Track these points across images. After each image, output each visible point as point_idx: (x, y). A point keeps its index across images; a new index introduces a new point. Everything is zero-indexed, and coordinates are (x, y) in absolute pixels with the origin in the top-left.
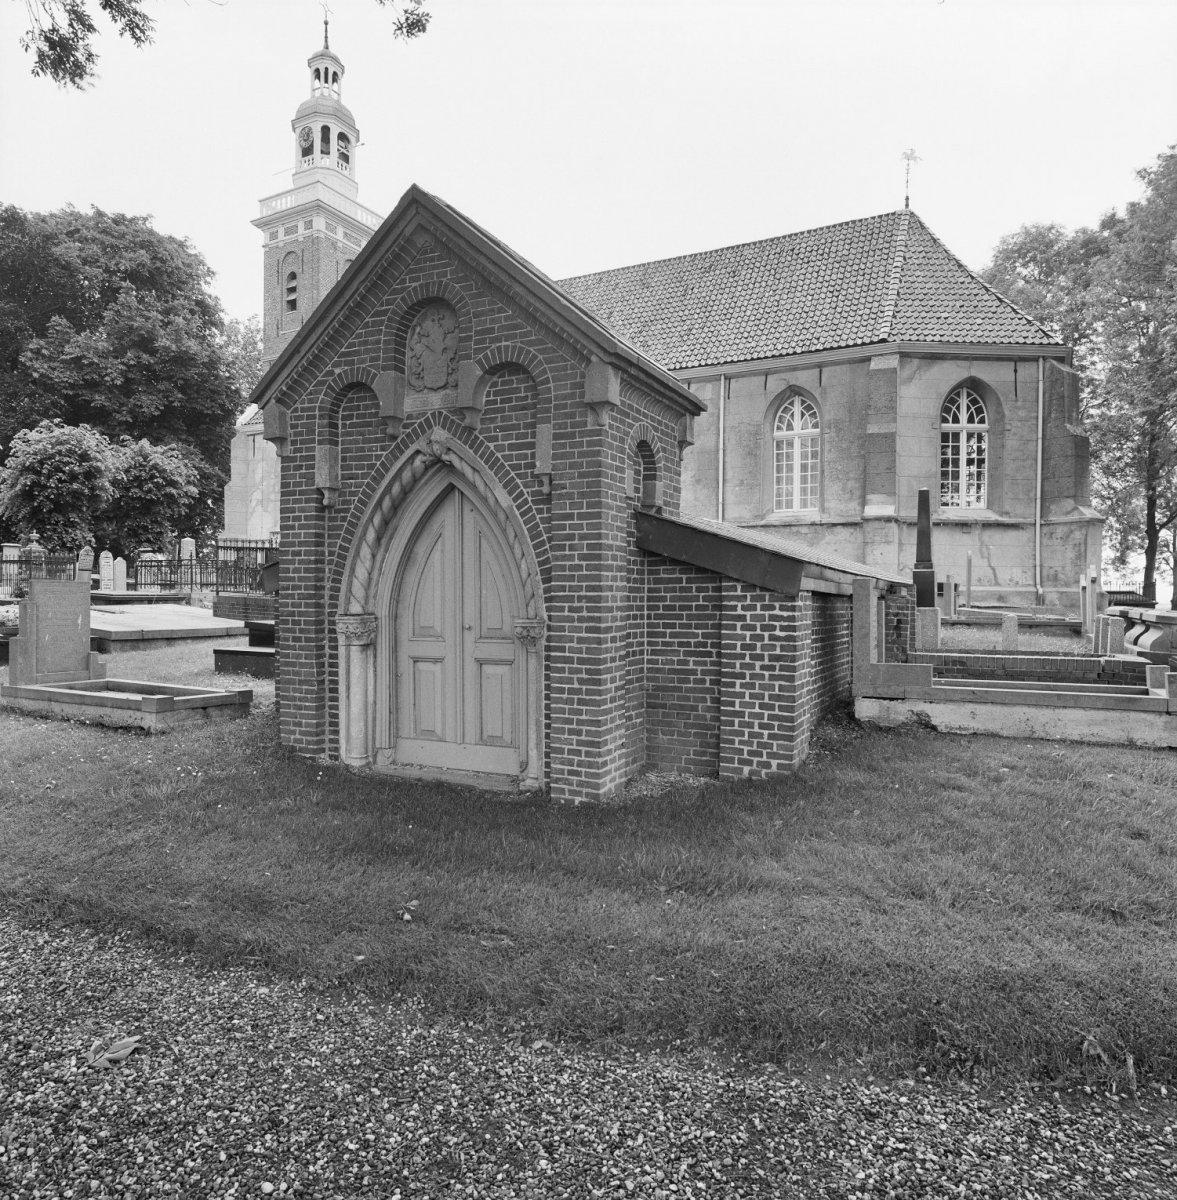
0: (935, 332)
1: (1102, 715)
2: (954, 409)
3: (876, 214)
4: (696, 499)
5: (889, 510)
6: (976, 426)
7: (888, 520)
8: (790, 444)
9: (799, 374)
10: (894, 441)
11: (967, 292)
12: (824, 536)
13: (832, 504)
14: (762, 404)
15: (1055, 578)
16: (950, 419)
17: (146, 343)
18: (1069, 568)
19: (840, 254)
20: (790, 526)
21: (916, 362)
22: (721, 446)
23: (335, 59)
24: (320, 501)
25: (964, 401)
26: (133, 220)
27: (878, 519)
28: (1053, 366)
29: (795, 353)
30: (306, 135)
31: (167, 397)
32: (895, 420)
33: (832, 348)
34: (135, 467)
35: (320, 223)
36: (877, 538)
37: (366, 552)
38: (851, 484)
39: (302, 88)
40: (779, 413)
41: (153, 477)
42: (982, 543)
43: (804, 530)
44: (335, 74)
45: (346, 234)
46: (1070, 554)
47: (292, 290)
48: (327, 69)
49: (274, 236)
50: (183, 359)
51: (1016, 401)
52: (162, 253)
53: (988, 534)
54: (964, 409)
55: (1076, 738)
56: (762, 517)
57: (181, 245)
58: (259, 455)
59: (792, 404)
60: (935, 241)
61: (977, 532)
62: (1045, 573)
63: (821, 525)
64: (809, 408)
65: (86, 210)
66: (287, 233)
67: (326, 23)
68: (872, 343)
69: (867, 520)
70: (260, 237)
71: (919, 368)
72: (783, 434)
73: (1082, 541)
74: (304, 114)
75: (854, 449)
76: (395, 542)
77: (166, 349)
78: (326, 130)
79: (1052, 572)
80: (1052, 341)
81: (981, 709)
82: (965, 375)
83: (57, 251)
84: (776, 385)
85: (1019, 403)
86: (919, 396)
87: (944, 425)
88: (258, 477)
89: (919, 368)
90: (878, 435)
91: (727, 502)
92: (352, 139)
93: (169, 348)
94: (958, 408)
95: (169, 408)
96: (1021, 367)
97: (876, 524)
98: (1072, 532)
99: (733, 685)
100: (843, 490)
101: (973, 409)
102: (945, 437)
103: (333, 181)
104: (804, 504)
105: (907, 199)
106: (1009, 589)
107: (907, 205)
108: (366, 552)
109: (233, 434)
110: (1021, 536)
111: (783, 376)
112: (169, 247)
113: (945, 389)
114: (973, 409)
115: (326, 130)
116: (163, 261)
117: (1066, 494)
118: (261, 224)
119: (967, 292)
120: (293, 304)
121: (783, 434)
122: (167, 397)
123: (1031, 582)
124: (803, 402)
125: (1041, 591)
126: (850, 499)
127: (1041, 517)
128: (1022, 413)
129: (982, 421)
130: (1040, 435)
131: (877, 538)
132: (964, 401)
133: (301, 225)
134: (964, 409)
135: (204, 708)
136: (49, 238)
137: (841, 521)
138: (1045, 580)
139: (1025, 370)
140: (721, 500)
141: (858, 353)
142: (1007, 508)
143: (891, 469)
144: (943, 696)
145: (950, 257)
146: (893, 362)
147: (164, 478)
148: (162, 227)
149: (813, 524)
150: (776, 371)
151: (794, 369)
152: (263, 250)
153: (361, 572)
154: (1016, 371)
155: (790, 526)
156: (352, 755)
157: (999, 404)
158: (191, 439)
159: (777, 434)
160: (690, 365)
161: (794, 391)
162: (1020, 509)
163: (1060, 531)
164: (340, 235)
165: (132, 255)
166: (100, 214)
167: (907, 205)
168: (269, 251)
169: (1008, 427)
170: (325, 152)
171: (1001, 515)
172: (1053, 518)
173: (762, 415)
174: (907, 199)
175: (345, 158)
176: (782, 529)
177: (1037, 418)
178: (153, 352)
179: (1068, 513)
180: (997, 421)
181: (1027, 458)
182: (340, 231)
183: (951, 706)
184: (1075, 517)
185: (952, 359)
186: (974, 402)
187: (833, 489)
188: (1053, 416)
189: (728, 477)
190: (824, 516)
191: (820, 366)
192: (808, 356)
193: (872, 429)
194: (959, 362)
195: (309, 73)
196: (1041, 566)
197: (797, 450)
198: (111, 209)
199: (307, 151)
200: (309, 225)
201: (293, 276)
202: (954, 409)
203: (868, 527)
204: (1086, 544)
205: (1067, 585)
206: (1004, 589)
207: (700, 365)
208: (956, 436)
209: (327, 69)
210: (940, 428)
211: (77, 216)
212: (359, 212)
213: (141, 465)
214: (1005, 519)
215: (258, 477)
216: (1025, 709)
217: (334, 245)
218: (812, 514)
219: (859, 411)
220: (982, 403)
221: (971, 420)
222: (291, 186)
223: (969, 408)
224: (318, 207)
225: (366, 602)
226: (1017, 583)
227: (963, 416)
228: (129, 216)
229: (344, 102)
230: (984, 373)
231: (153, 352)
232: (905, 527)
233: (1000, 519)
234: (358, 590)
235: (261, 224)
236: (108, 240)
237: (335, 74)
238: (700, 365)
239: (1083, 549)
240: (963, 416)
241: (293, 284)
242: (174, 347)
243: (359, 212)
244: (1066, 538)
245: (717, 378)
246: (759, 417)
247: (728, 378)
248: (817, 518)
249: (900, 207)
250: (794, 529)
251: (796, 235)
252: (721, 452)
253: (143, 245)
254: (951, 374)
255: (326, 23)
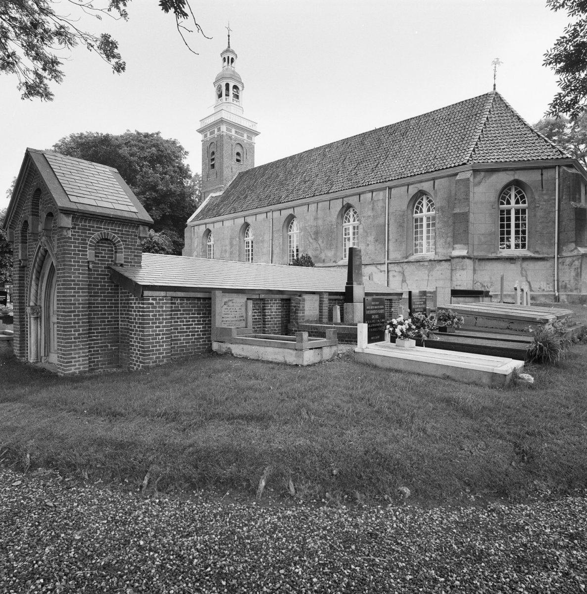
0: (494, 157)
1: (277, 350)
2: (507, 197)
3: (478, 95)
4: (376, 250)
5: (464, 253)
6: (521, 205)
7: (463, 257)
8: (422, 220)
9: (423, 184)
10: (467, 216)
11: (520, 133)
12: (436, 266)
13: (439, 250)
14: (406, 201)
15: (565, 287)
16: (505, 203)
17: (154, 188)
18: (572, 281)
19: (455, 119)
20: (419, 261)
21: (483, 174)
22: (387, 223)
23: (233, 52)
24: (20, 264)
25: (513, 193)
26: (152, 135)
27: (458, 257)
28: (564, 170)
29: (421, 173)
30: (219, 89)
31: (163, 211)
32: (468, 205)
33: (439, 170)
34: (147, 243)
35: (224, 128)
36: (458, 267)
37: (33, 283)
38: (449, 239)
39: (218, 66)
40: (416, 205)
41: (154, 247)
42: (522, 268)
43: (426, 264)
44: (232, 59)
45: (236, 132)
46: (573, 274)
47: (213, 160)
48: (228, 57)
49: (206, 136)
50: (171, 193)
51: (543, 191)
52: (163, 149)
53: (525, 264)
54: (351, 216)
55: (270, 360)
56: (407, 258)
57: (174, 143)
58: (196, 236)
59: (422, 199)
60: (507, 106)
61: (519, 263)
62: (560, 284)
63: (435, 261)
64: (519, 193)
65: (133, 132)
66: (210, 134)
67: (229, 36)
68: (459, 165)
69: (453, 258)
70: (200, 137)
71: (485, 177)
72: (419, 215)
73: (579, 266)
74: (219, 79)
75: (450, 222)
76: (43, 278)
77: (162, 190)
78: (227, 85)
79: (564, 283)
80: (564, 156)
81: (246, 347)
82: (512, 178)
83: (120, 151)
84: (413, 190)
85: (544, 192)
86: (484, 192)
87: (501, 206)
88: (196, 245)
89: (485, 177)
90: (459, 214)
91: (390, 251)
92: (240, 88)
93: (162, 189)
94: (422, 206)
95: (164, 215)
96: (545, 172)
97: (457, 260)
98: (574, 261)
99: (83, 330)
100: (445, 242)
101: (518, 196)
102: (502, 211)
103: (233, 109)
104: (428, 251)
105: (495, 85)
106: (538, 293)
107: (494, 89)
108: (33, 283)
109: (186, 226)
110: (548, 264)
111: (416, 185)
112: (165, 145)
113: (500, 186)
114: (518, 196)
115: (227, 85)
116: (162, 151)
117: (571, 240)
118: (201, 131)
119: (520, 133)
120: (213, 166)
121: (419, 215)
122: (163, 211)
123: (552, 290)
124: (428, 198)
125: (557, 294)
126: (449, 247)
127: (558, 254)
128: (546, 197)
129: (524, 202)
130: (557, 208)
131: (458, 267)
132: (513, 193)
133: (216, 130)
134: (351, 216)
135: (8, 341)
136: (119, 146)
137: (445, 258)
138: (560, 288)
139: (547, 174)
140: (386, 250)
141: (451, 171)
142: (537, 249)
143: (466, 231)
144: (241, 342)
145: (513, 114)
146: (468, 174)
147: (159, 247)
148: (165, 136)
149: (430, 261)
150: (412, 184)
151: (421, 182)
152: (201, 143)
153: (33, 291)
154: (542, 174)
155: (419, 261)
156: (32, 359)
157: (532, 193)
158: (175, 229)
159: (415, 215)
160: (372, 183)
161: (421, 193)
162: (545, 250)
163: (568, 260)
164: (233, 132)
165: (149, 150)
166: (138, 133)
167: (494, 89)
168: (204, 142)
169: (538, 205)
170: (227, 95)
171: (534, 253)
172: (564, 254)
173: (406, 206)
174: (495, 85)
175: (237, 97)
176: (415, 263)
177: (555, 199)
178: (156, 191)
179: (572, 251)
180: (532, 202)
181: (550, 221)
182: (233, 130)
183: (237, 345)
184: (575, 253)
185: (503, 171)
186: (519, 193)
187: (440, 242)
188: (564, 197)
189: (391, 237)
190: (437, 256)
191: (434, 179)
192: (428, 174)
193: (457, 211)
194: (508, 172)
195: (221, 59)
196: (558, 281)
197: (425, 223)
198: (143, 131)
199: (220, 96)
200: (219, 129)
201: (213, 153)
202: (420, 206)
203: (454, 261)
204: (581, 268)
205: (571, 291)
206: (535, 293)
207: (377, 183)
208: (509, 212)
209: (228, 57)
210: (499, 208)
211: (131, 135)
212: (243, 121)
213: (150, 242)
214: (536, 255)
215: (196, 245)
216: (257, 347)
217: (230, 137)
218: (431, 255)
219: (451, 201)
220: (524, 193)
221: (517, 202)
222: (214, 112)
223: (516, 196)
224: (222, 121)
225: (37, 301)
226: (544, 290)
227: (513, 201)
228: (150, 133)
229: (236, 71)
230: (522, 176)
231: (156, 191)
232: (477, 261)
233: (533, 255)
234: (32, 298)
235: (201, 131)
236: (141, 144)
237: (232, 59)
238: (377, 183)
239: (579, 270)
240: (513, 201)
241: (213, 157)
242: (165, 189)
243: (243, 121)
244: (571, 265)
245: (385, 189)
246: (405, 207)
247: (390, 188)
248: (432, 258)
249: (490, 90)
250: (422, 263)
251: (437, 111)
252: (387, 225)
253: (154, 146)
254: (504, 178)
255: (229, 36)
